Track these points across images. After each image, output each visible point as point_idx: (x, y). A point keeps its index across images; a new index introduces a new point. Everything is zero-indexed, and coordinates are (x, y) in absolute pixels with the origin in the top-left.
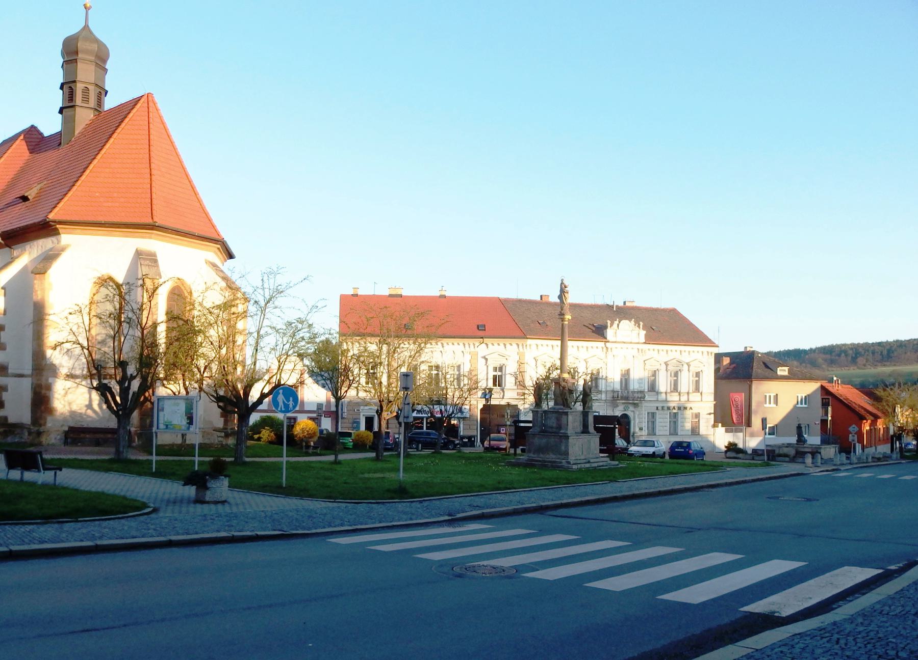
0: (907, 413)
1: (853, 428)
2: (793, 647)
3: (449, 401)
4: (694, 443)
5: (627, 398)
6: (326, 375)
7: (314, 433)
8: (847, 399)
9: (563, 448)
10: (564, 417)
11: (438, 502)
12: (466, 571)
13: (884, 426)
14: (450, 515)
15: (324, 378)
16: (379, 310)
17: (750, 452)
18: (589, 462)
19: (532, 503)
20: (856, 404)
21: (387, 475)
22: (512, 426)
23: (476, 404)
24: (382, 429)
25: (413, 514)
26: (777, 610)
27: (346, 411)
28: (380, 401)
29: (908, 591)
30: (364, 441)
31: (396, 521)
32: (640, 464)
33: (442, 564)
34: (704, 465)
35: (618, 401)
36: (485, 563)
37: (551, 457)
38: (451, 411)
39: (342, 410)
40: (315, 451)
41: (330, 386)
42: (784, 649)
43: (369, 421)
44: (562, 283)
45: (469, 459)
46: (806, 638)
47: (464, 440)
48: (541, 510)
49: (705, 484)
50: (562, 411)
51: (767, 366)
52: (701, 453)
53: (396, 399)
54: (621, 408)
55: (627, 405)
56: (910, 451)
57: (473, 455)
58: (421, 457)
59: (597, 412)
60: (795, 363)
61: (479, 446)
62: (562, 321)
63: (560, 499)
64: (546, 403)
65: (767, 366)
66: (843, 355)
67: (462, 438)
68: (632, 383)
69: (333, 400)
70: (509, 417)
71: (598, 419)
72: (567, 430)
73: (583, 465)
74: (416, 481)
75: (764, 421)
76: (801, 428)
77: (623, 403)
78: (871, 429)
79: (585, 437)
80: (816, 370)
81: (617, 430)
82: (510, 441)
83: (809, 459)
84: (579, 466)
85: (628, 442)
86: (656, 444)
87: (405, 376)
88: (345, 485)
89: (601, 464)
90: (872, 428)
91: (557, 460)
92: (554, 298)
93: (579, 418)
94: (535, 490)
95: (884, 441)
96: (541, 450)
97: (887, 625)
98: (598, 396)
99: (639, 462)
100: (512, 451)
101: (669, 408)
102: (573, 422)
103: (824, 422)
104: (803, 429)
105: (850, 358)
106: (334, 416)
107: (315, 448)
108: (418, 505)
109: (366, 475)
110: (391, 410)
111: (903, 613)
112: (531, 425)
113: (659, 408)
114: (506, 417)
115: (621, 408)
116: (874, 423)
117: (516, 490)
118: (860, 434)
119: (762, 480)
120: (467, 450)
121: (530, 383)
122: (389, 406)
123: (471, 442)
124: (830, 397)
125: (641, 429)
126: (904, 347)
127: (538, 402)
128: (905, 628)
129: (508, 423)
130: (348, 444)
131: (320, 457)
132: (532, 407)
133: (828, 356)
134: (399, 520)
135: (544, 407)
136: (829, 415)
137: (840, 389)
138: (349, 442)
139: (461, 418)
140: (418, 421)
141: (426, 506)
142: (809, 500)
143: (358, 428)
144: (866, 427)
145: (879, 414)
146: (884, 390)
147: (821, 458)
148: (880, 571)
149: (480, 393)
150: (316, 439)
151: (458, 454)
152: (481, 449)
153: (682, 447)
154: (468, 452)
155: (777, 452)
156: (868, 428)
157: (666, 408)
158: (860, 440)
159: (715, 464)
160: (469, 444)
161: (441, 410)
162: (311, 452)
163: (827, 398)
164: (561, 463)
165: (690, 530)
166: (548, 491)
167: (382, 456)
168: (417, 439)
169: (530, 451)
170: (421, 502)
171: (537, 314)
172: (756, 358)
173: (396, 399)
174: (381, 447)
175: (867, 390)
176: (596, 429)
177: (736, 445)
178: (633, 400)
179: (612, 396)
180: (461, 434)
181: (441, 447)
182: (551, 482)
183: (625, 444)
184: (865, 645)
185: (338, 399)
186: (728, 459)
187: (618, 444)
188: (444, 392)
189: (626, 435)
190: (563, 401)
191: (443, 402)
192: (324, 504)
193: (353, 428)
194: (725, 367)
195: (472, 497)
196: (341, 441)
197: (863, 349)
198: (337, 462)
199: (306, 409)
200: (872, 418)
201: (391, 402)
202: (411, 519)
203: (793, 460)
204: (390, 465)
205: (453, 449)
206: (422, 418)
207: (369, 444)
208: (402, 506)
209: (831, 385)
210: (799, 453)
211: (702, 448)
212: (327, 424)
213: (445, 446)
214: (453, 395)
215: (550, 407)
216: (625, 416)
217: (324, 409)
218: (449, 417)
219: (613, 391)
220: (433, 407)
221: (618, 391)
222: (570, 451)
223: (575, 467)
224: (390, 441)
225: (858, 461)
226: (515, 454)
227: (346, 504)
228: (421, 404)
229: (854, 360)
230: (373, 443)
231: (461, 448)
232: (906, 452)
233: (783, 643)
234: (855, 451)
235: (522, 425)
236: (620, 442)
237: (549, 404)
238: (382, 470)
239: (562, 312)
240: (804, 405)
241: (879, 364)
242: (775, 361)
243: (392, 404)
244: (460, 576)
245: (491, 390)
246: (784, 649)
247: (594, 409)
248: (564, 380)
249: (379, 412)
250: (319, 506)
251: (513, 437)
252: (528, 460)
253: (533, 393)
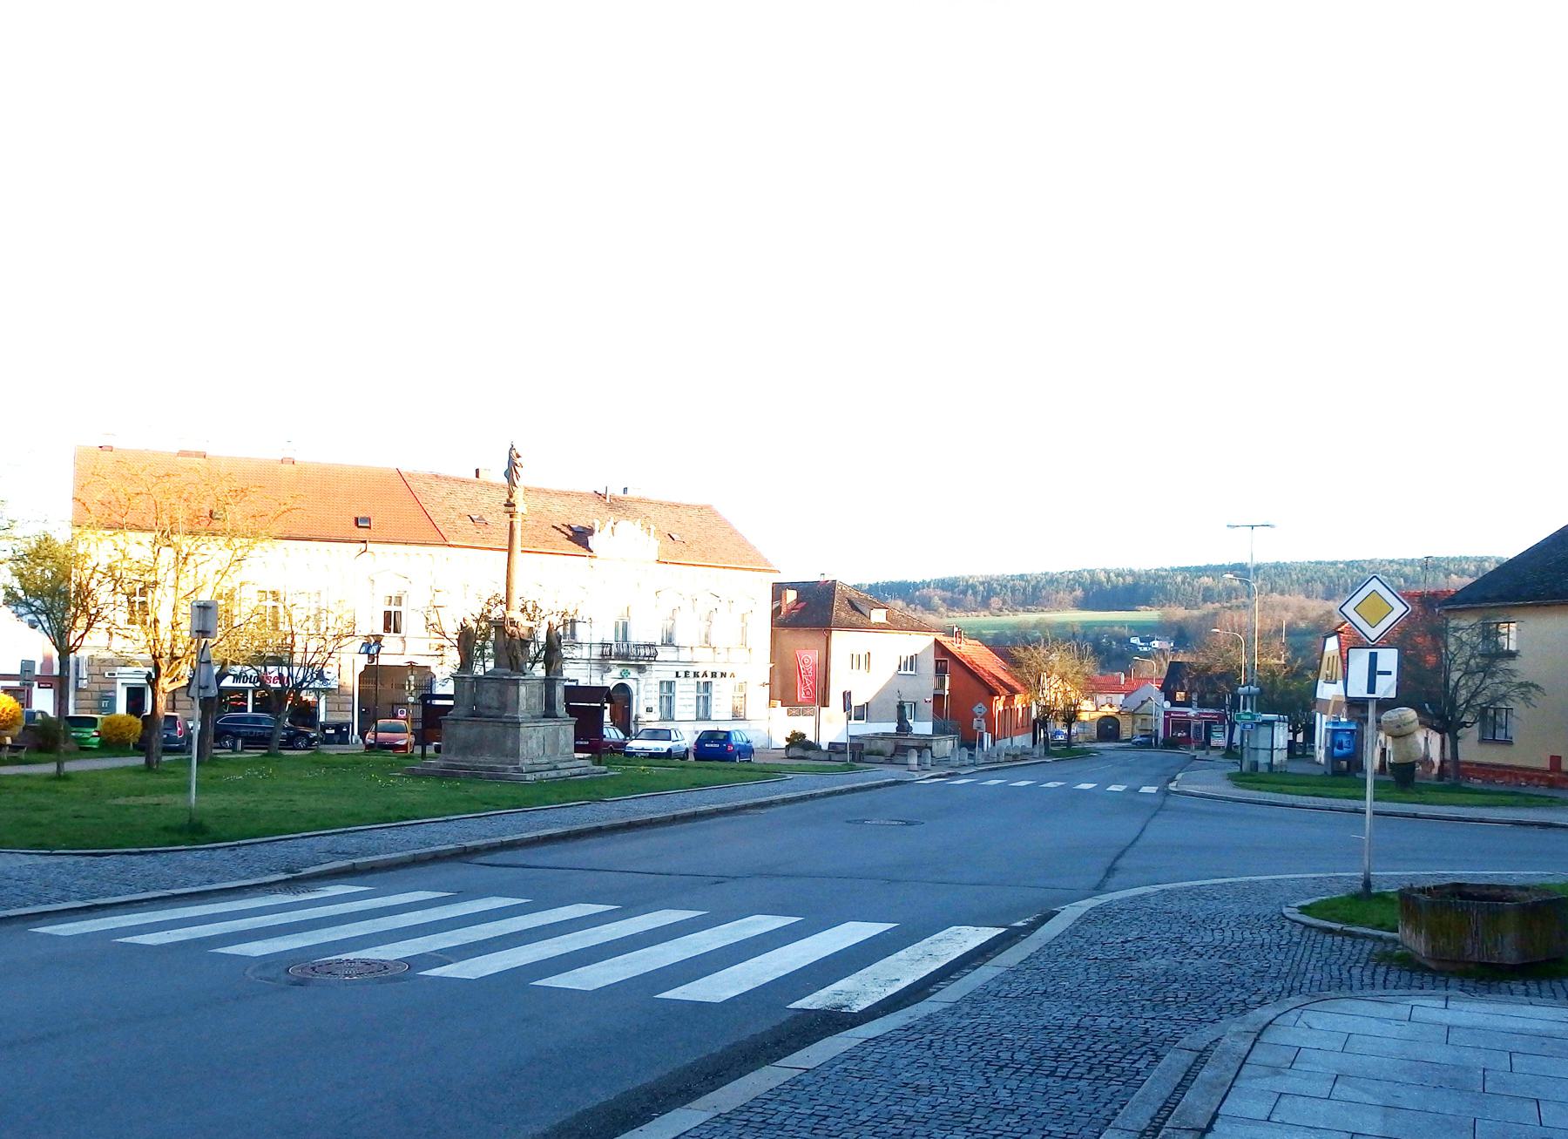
0: (1056, 686)
1: (979, 709)
2: (863, 1060)
3: (297, 658)
4: (737, 733)
5: (626, 657)
6: (38, 603)
7: (14, 719)
8: (972, 663)
9: (509, 744)
10: (512, 688)
11: (267, 848)
12: (313, 973)
13: (1024, 706)
14: (288, 871)
15: (34, 609)
16: (154, 480)
17: (825, 747)
18: (555, 768)
19: (449, 843)
20: (985, 671)
21: (167, 799)
22: (419, 704)
23: (347, 670)
24: (159, 711)
25: (216, 872)
26: (845, 1003)
27: (85, 677)
28: (154, 656)
29: (1037, 958)
30: (122, 733)
31: (180, 887)
32: (643, 770)
33: (266, 961)
34: (751, 770)
35: (611, 662)
36: (351, 956)
37: (487, 760)
38: (301, 676)
39: (77, 674)
40: (15, 755)
41: (46, 625)
42: (850, 1065)
43: (135, 695)
44: (512, 448)
45: (330, 765)
46: (883, 1044)
47: (327, 731)
48: (464, 855)
49: (751, 801)
50: (507, 677)
51: (854, 607)
52: (747, 750)
53: (188, 653)
54: (616, 672)
56: (1059, 743)
57: (344, 759)
58: (238, 762)
59: (574, 681)
60: (900, 603)
61: (357, 742)
62: (511, 516)
63: (500, 836)
64: (481, 663)
65: (854, 607)
66: (970, 592)
67: (325, 727)
69: (55, 654)
70: (412, 688)
71: (574, 692)
72: (517, 713)
73: (544, 774)
74: (225, 809)
75: (847, 696)
76: (904, 707)
77: (619, 665)
78: (1005, 710)
79: (550, 724)
80: (931, 616)
81: (607, 713)
82: (414, 732)
83: (913, 760)
84: (538, 774)
85: (627, 732)
86: (673, 737)
87: (202, 610)
88: (76, 821)
89: (576, 771)
90: (1007, 708)
91: (498, 766)
92: (495, 473)
93: (539, 691)
94: (453, 820)
95: (1020, 730)
96: (467, 748)
97: (1003, 1013)
98: (574, 651)
99: (642, 768)
100: (418, 750)
102: (527, 697)
103: (938, 698)
104: (907, 710)
105: (979, 599)
106: (56, 684)
107: (14, 748)
108: (227, 855)
109: (121, 801)
110: (178, 675)
111: (1027, 993)
112: (451, 703)
113: (682, 674)
114: (407, 688)
115: (616, 672)
116: (1010, 700)
117: (420, 821)
118: (989, 717)
119: (841, 792)
120: (332, 750)
121: (452, 629)
122: (173, 665)
123: (341, 732)
125: (649, 710)
126: (1055, 583)
127: (466, 664)
128: (1027, 1017)
129: (411, 699)
130: (90, 740)
131: (24, 767)
132: (455, 671)
133: (949, 594)
134: (185, 885)
135: (478, 670)
136: (947, 687)
137: (967, 649)
138: (91, 736)
139: (322, 690)
140: (237, 696)
141: (243, 857)
142: (908, 824)
143: (112, 707)
144: (999, 705)
145: (1018, 686)
146: (1025, 649)
147: (932, 757)
148: (1002, 930)
149: (357, 644)
150: (17, 730)
151: (316, 758)
152: (361, 747)
153: (717, 741)
154: (334, 752)
155: (866, 747)
156: (1001, 708)
157: (691, 674)
158: (990, 729)
159: (771, 768)
160: (337, 738)
161: (281, 675)
162: (6, 758)
163: (945, 659)
164: (505, 770)
165: (720, 880)
166: (478, 820)
167: (157, 762)
168: (235, 731)
169: (449, 750)
170: (232, 848)
171: (469, 502)
172: (838, 593)
173: (188, 653)
174: (156, 745)
175: (1001, 646)
176: (570, 710)
177: (803, 736)
178: (637, 660)
179: (600, 653)
180: (323, 720)
181: (281, 743)
182: (486, 804)
183: (621, 736)
184: (969, 1047)
185: (65, 651)
186: (790, 760)
187: (608, 736)
188: (289, 640)
189: (624, 720)
190: (510, 659)
191: (286, 660)
192: (28, 860)
193: (101, 710)
194: (790, 607)
195: (335, 837)
196: (73, 734)
197: (999, 585)
198: (60, 777)
200: (1007, 692)
201: (177, 658)
202: (210, 882)
203: (890, 760)
204: (173, 780)
205: (304, 749)
206: (245, 691)
207: (133, 738)
208: (193, 857)
209: (950, 639)
210: (900, 746)
211: (748, 742)
212: (43, 701)
213: (290, 743)
214: (305, 647)
215: (487, 670)
216: (623, 688)
217: (37, 672)
218: (298, 688)
219: (603, 645)
220: (266, 670)
221: (611, 644)
222: (523, 749)
223: (529, 777)
224: (178, 733)
225: (986, 760)
226: (423, 755)
227: (76, 858)
228: (239, 664)
229: (985, 604)
230: (142, 739)
231: (322, 746)
232: (1052, 745)
233: (850, 1055)
234: (983, 744)
235: (438, 702)
236: (612, 733)
237: (485, 666)
238: (156, 790)
239: (512, 500)
240: (909, 672)
241: (1021, 609)
242: (867, 600)
243: (179, 663)
244: (302, 983)
245: (378, 640)
246: (850, 1065)
247: (566, 674)
248: (513, 623)
249: (153, 681)
250: (16, 864)
251: (419, 726)
252: (448, 766)
253: (457, 645)
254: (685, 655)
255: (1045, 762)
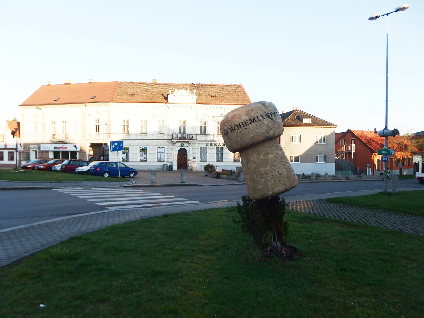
55: (183, 143)
68: (422, 176)
101: (215, 145)
124: (355, 138)
125: (194, 158)
157: (213, 145)
199: (8, 147)
240: (322, 143)
254: (209, 138)
255: (375, 180)
